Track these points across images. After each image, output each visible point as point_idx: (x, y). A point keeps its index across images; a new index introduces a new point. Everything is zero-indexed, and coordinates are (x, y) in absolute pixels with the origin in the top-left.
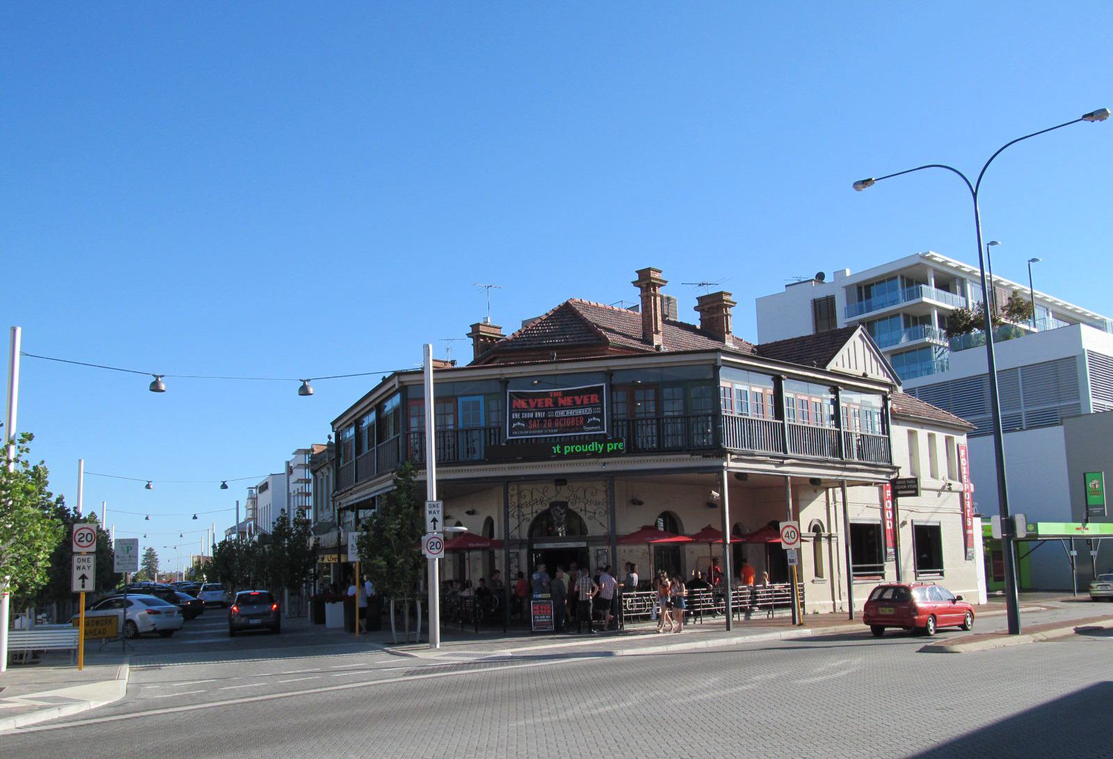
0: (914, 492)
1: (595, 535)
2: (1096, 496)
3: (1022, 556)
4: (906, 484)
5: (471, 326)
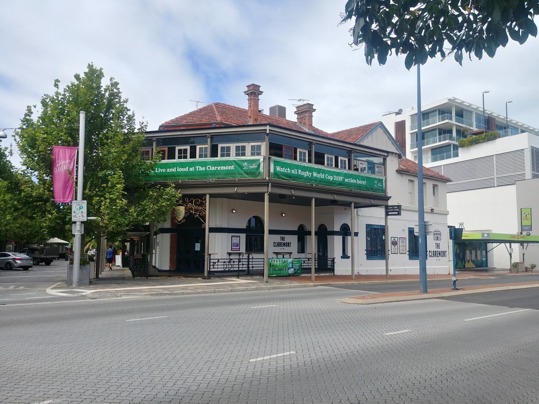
0: (397, 213)
1: (226, 234)
2: (526, 221)
3: (488, 251)
4: (393, 209)
5: (247, 86)
